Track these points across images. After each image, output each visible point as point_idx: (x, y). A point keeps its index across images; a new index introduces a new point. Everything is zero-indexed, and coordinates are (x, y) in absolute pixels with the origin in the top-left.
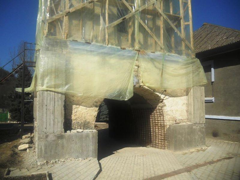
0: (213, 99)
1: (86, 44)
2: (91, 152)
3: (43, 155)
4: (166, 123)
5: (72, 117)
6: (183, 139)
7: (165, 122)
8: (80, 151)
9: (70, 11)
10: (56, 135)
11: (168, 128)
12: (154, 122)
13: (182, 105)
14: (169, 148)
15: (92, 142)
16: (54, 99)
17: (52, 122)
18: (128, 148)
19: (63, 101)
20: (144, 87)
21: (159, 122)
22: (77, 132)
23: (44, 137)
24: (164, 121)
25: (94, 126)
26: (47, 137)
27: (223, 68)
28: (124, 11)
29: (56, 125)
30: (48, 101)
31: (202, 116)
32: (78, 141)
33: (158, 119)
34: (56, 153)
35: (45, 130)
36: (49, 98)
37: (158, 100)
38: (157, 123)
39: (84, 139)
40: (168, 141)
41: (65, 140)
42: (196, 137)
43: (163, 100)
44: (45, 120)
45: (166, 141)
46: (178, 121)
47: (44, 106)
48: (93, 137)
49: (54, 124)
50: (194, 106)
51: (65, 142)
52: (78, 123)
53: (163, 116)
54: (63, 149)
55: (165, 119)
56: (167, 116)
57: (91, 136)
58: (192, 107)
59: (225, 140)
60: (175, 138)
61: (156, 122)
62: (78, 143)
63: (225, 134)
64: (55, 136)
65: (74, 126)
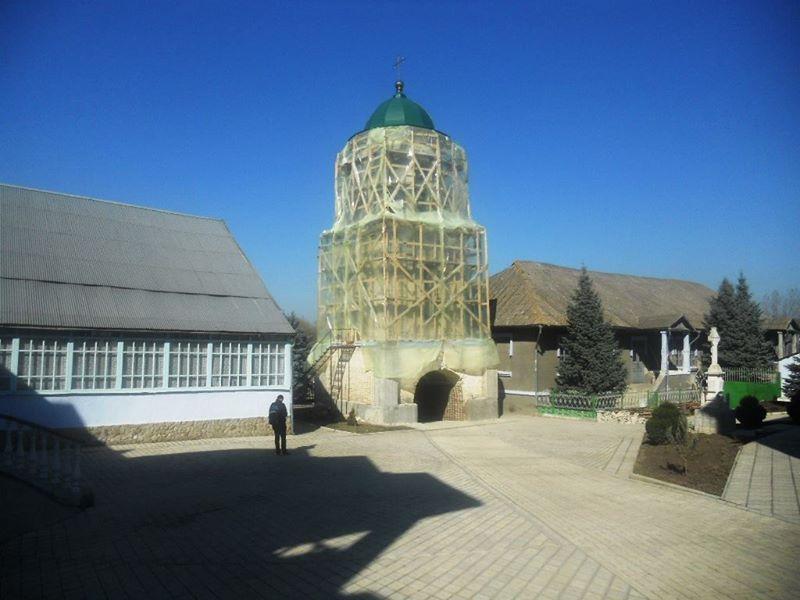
0: (510, 373)
14: (467, 419)
25: (337, 268)
37: (457, 378)
60: (472, 411)
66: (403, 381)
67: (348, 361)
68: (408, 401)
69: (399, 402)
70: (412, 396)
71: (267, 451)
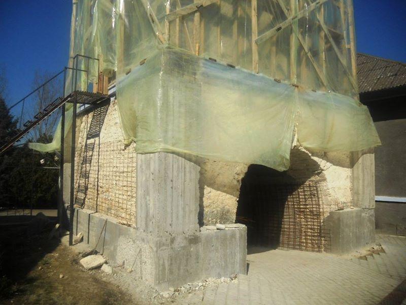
1: (228, 68)
2: (238, 265)
3: (167, 276)
4: (323, 209)
5: (203, 202)
6: (351, 234)
7: (321, 207)
8: (223, 263)
9: (203, 4)
10: (187, 236)
11: (328, 217)
12: (296, 206)
13: (346, 179)
15: (239, 246)
16: (183, 169)
17: (181, 213)
18: (260, 254)
19: (198, 173)
20: (300, 148)
21: (308, 207)
22: (218, 229)
23: (169, 241)
24: (319, 205)
26: (172, 241)
27: (388, 121)
28: (280, 15)
29: (187, 218)
30: (175, 173)
31: (370, 197)
32: (221, 246)
33: (305, 201)
34: (188, 270)
35: (169, 229)
36: (175, 166)
38: (303, 208)
39: (228, 242)
40: (328, 239)
41: (200, 246)
42: (365, 231)
43: (323, 170)
44: (169, 210)
45: (323, 239)
46: (341, 206)
47: (169, 182)
48: (241, 235)
49: (184, 217)
50: (363, 180)
51: (200, 250)
52: (213, 212)
53: (318, 197)
54: (198, 262)
55: (321, 203)
56: (327, 197)
57: (238, 236)
58: (361, 182)
59: (390, 234)
60: (329, 234)
61: (302, 207)
62: (221, 249)
63: (390, 225)
64: (186, 238)
65: (207, 219)
66: (208, 167)
67: (98, 135)
68: (223, 217)
69: (201, 224)
70: (231, 202)
71: (376, 158)
